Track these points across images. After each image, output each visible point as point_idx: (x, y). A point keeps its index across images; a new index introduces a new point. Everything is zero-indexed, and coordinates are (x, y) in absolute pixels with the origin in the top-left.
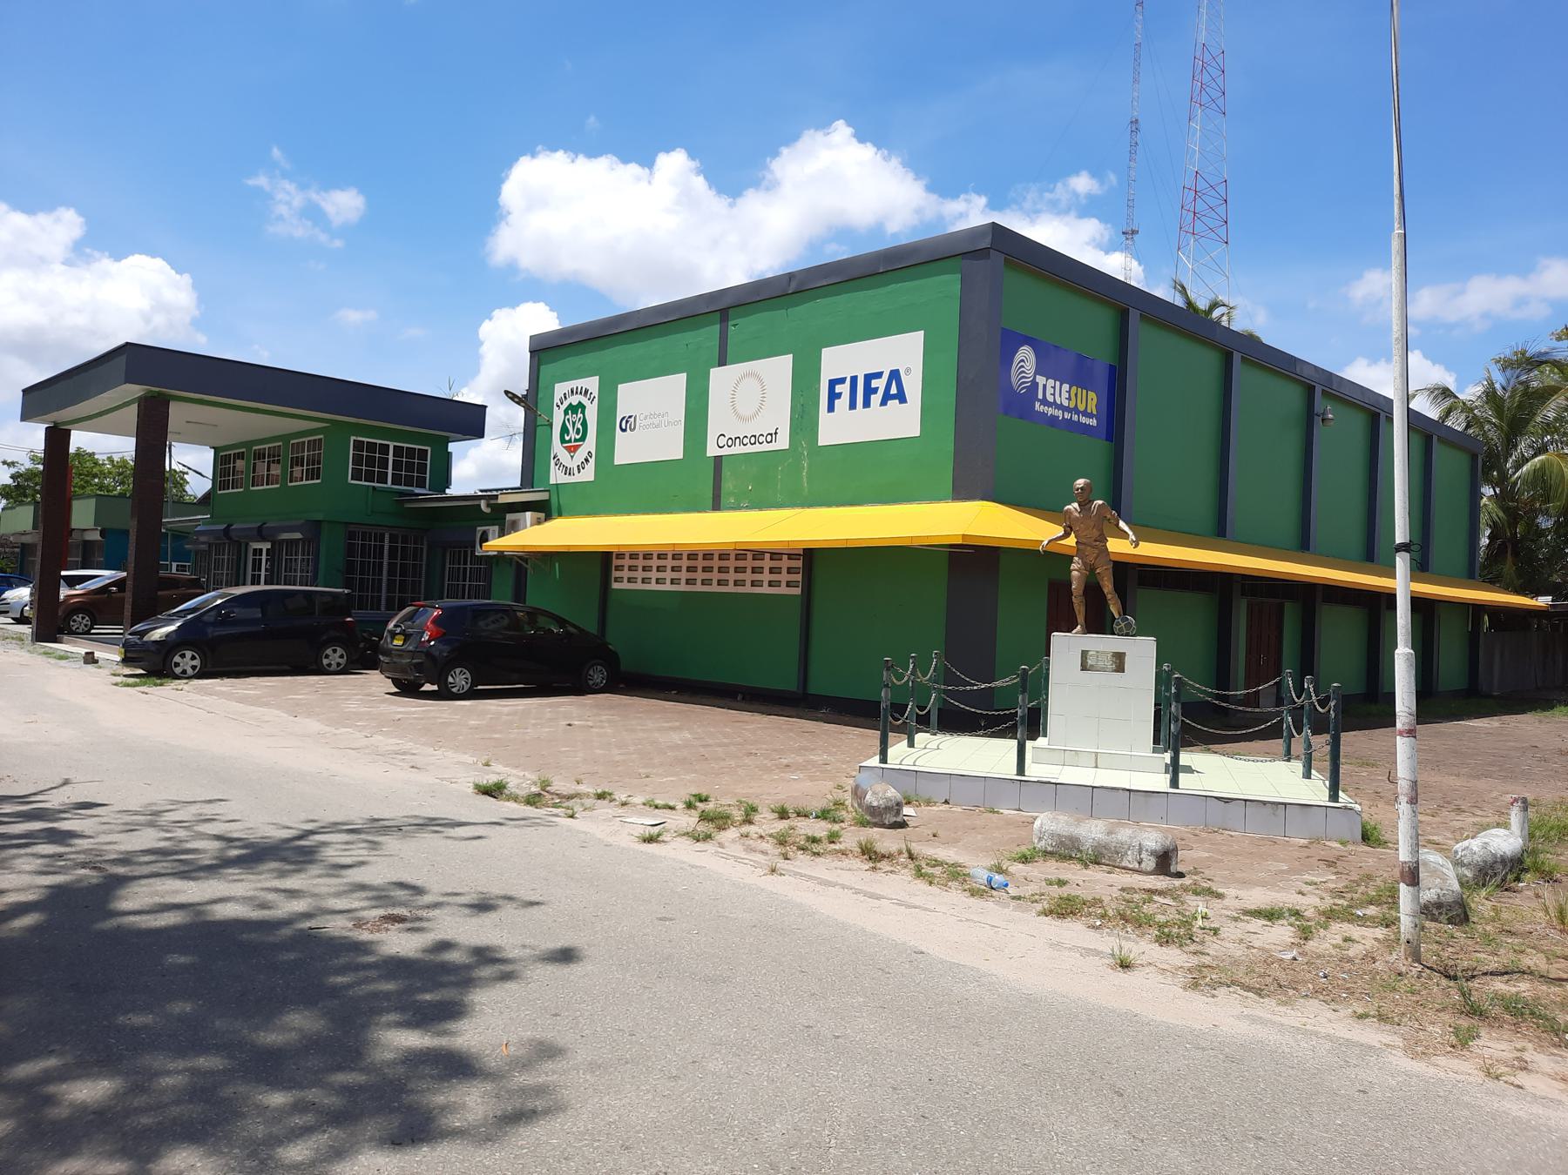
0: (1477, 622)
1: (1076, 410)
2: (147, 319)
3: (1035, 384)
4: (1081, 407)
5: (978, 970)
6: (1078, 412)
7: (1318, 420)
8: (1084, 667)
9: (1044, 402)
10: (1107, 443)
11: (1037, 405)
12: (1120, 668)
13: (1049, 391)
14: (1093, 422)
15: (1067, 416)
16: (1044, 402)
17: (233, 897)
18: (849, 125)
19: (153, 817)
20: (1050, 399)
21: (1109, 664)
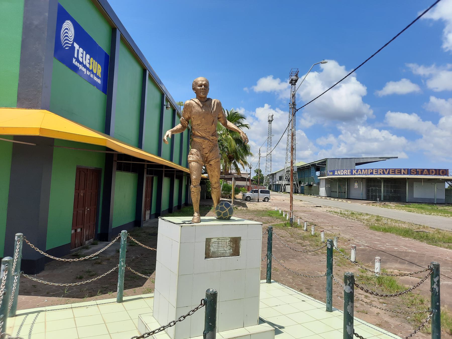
0: (203, 205)
1: (91, 71)
2: (180, 104)
3: (73, 48)
4: (95, 72)
5: (427, 243)
6: (93, 73)
7: (165, 107)
8: (208, 255)
9: (77, 60)
10: (103, 94)
11: (74, 60)
12: (236, 253)
13: (80, 55)
14: (99, 81)
15: (88, 73)
16: (77, 60)
17: (394, 322)
18: (269, 105)
19: (446, 216)
20: (81, 59)
21: (229, 250)
